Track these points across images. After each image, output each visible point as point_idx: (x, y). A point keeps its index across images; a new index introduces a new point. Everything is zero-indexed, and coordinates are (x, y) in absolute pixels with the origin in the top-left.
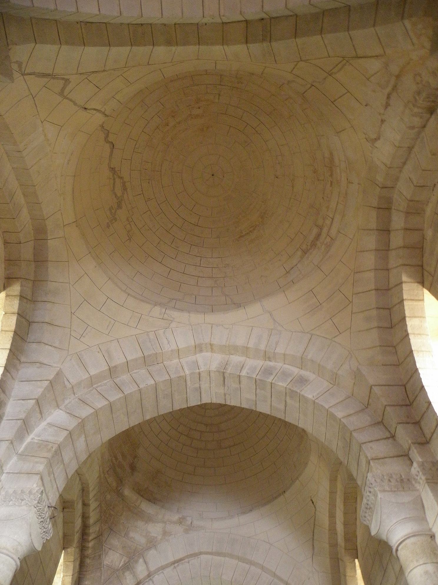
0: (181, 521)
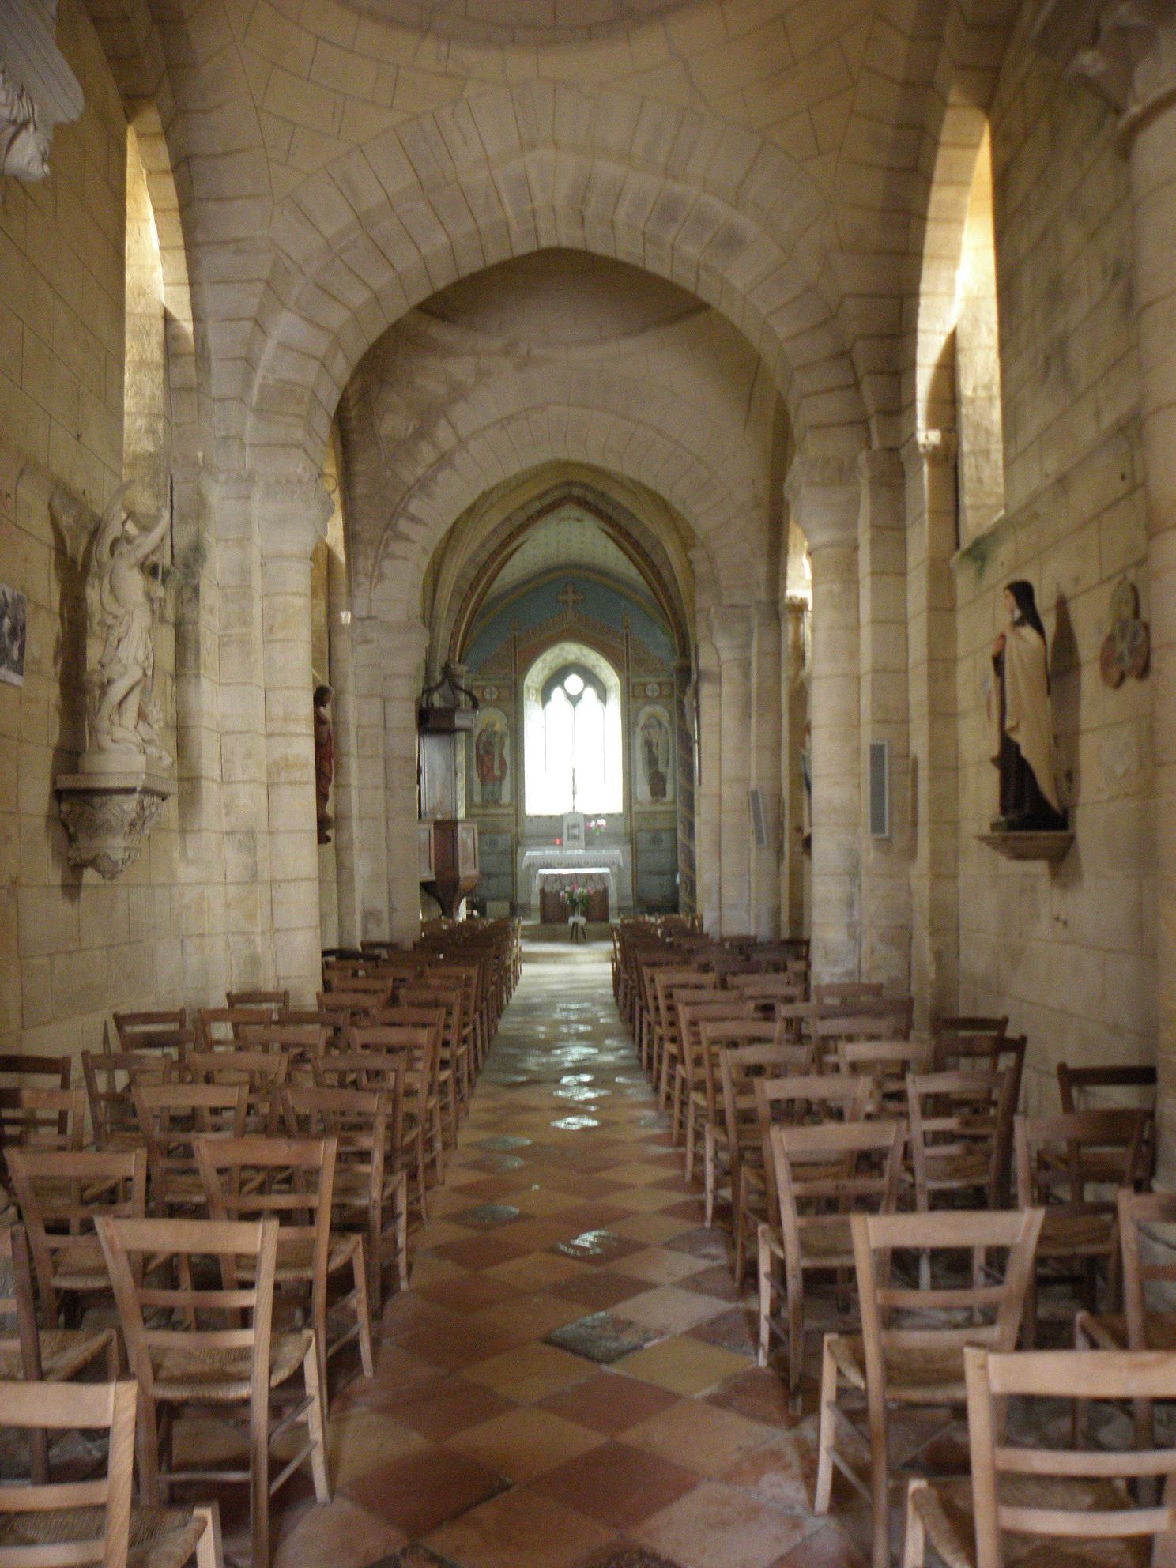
0: (507, 351)
